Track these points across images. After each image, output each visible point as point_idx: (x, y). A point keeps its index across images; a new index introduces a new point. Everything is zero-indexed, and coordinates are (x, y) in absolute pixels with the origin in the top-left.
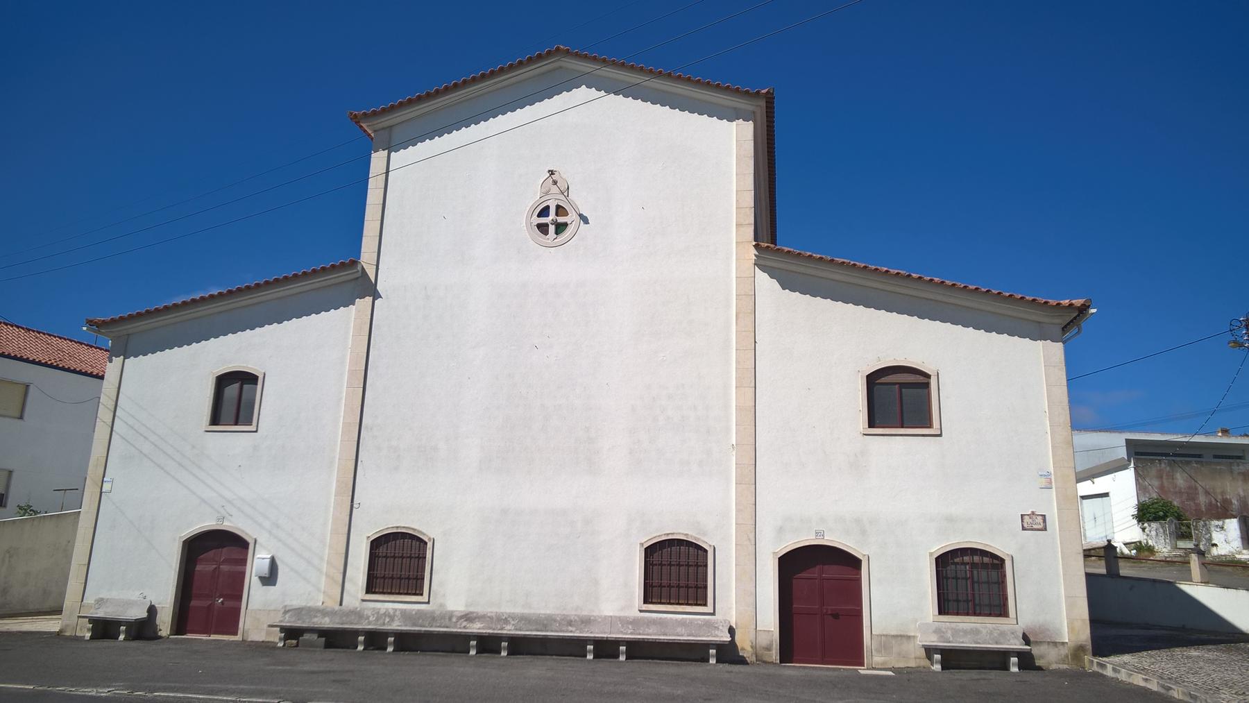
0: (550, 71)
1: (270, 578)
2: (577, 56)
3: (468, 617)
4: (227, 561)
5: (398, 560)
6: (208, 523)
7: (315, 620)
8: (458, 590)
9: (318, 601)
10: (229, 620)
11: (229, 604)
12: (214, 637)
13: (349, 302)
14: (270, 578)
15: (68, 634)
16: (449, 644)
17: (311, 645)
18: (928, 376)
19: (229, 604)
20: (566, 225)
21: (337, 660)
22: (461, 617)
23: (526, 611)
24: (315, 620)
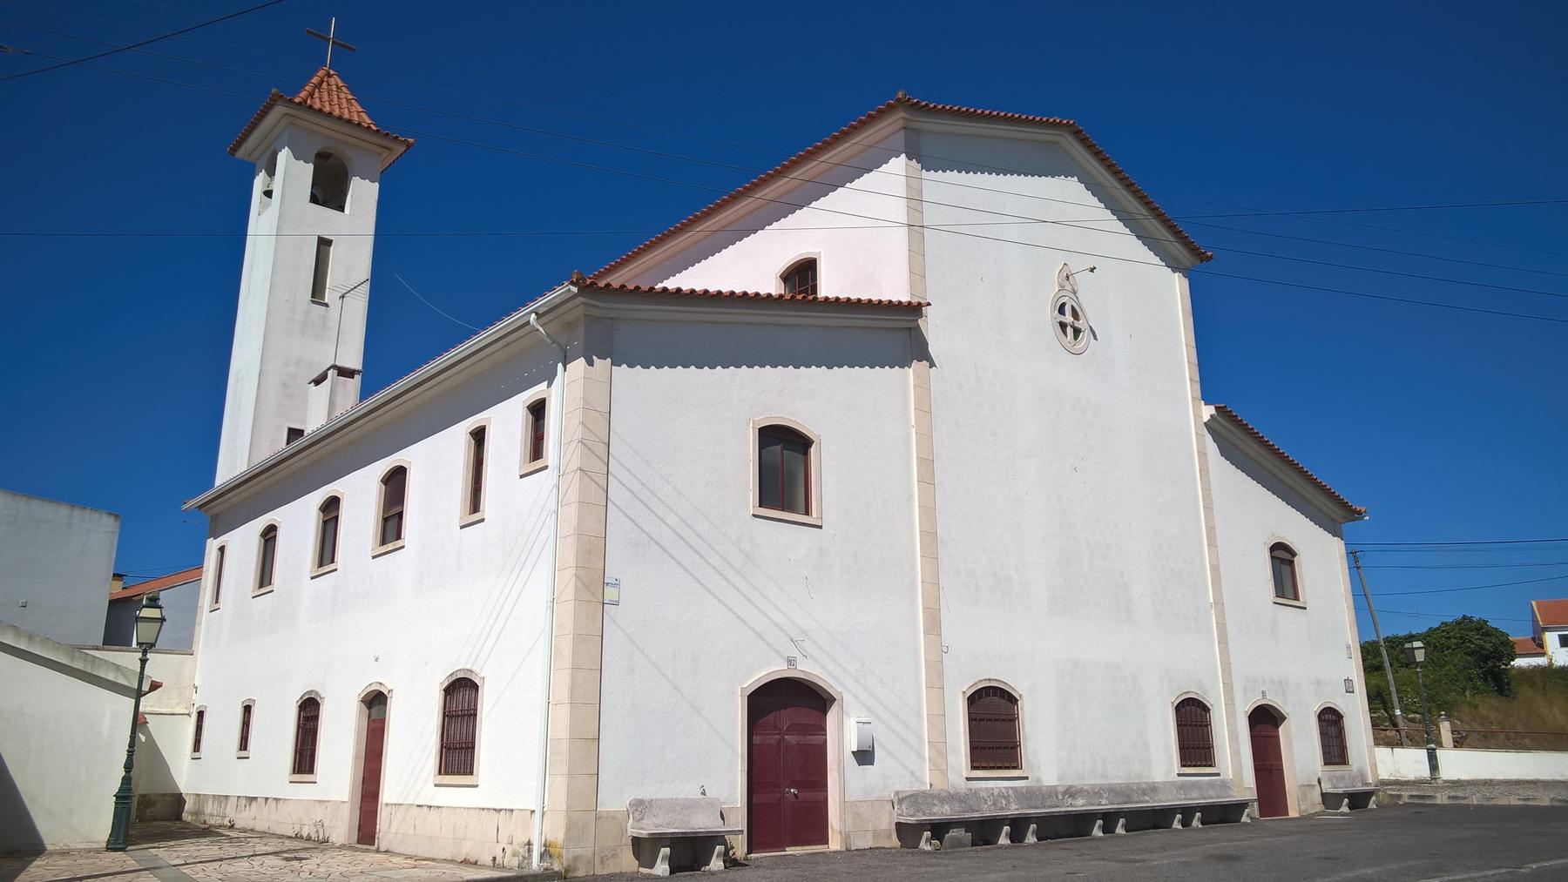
0: (979, 136)
1: (864, 756)
2: (1084, 141)
3: (1071, 792)
4: (789, 730)
5: (993, 722)
6: (774, 669)
7: (935, 809)
8: (1061, 756)
9: (926, 779)
10: (812, 824)
11: (806, 795)
12: (790, 851)
13: (904, 364)
14: (864, 756)
15: (580, 873)
16: (1067, 827)
17: (958, 844)
18: (399, 537)
19: (806, 795)
20: (1065, 333)
21: (1064, 857)
22: (1064, 793)
23: (1104, 782)
24: (935, 809)
